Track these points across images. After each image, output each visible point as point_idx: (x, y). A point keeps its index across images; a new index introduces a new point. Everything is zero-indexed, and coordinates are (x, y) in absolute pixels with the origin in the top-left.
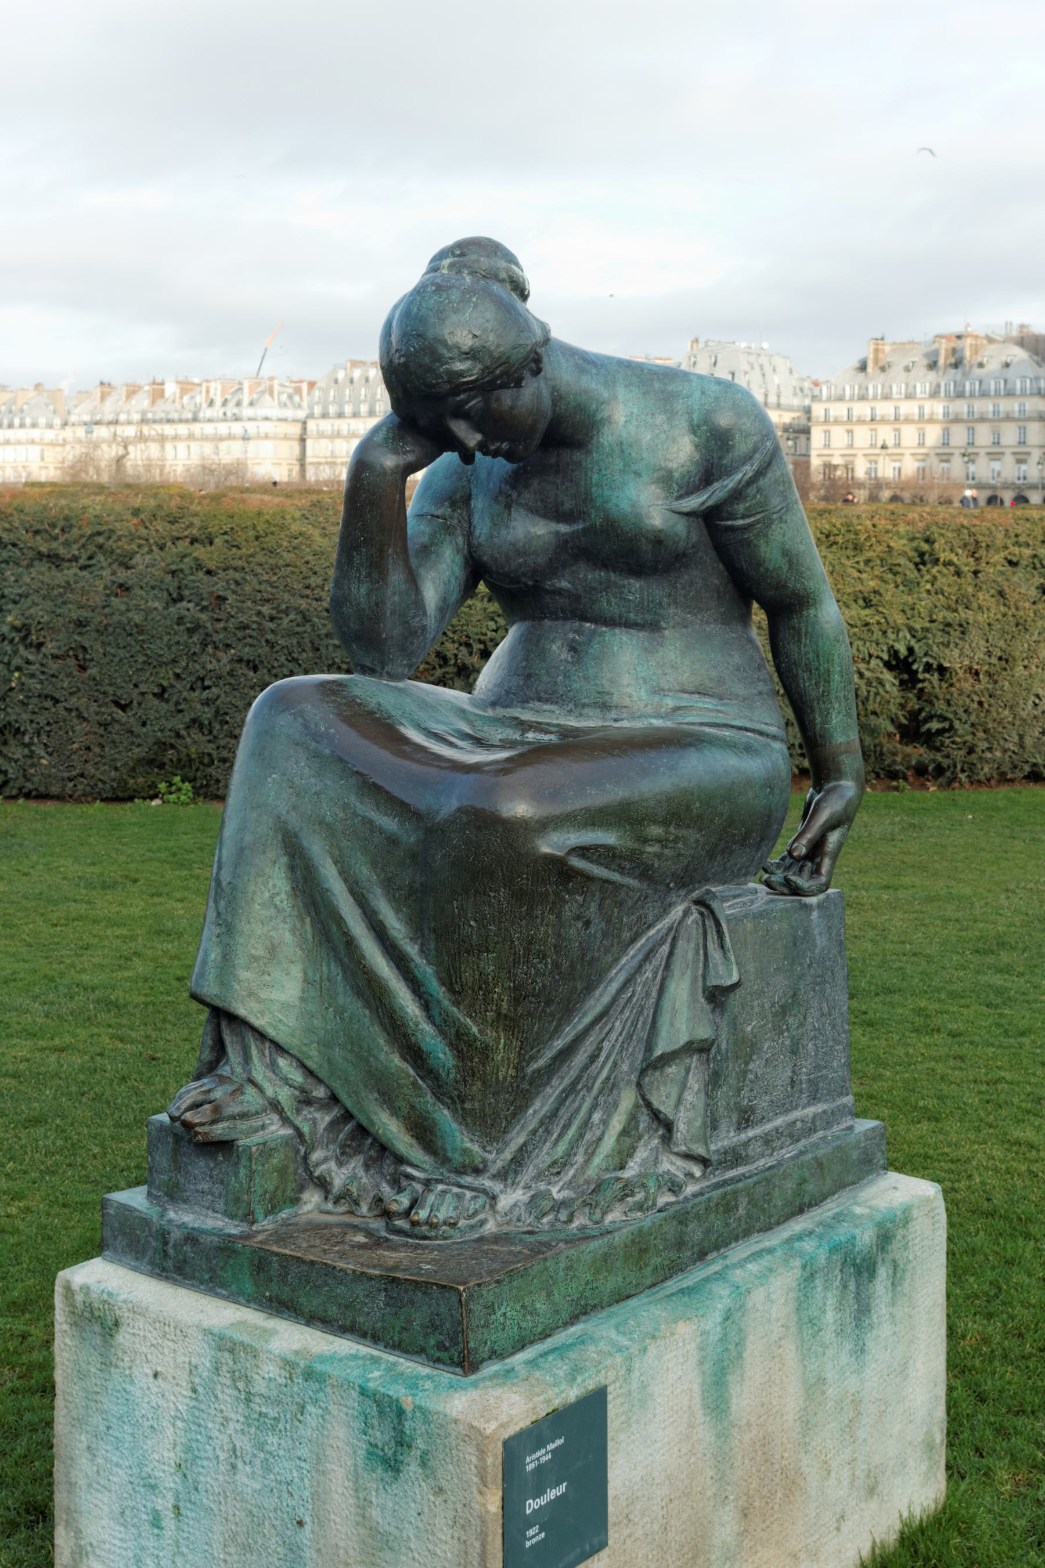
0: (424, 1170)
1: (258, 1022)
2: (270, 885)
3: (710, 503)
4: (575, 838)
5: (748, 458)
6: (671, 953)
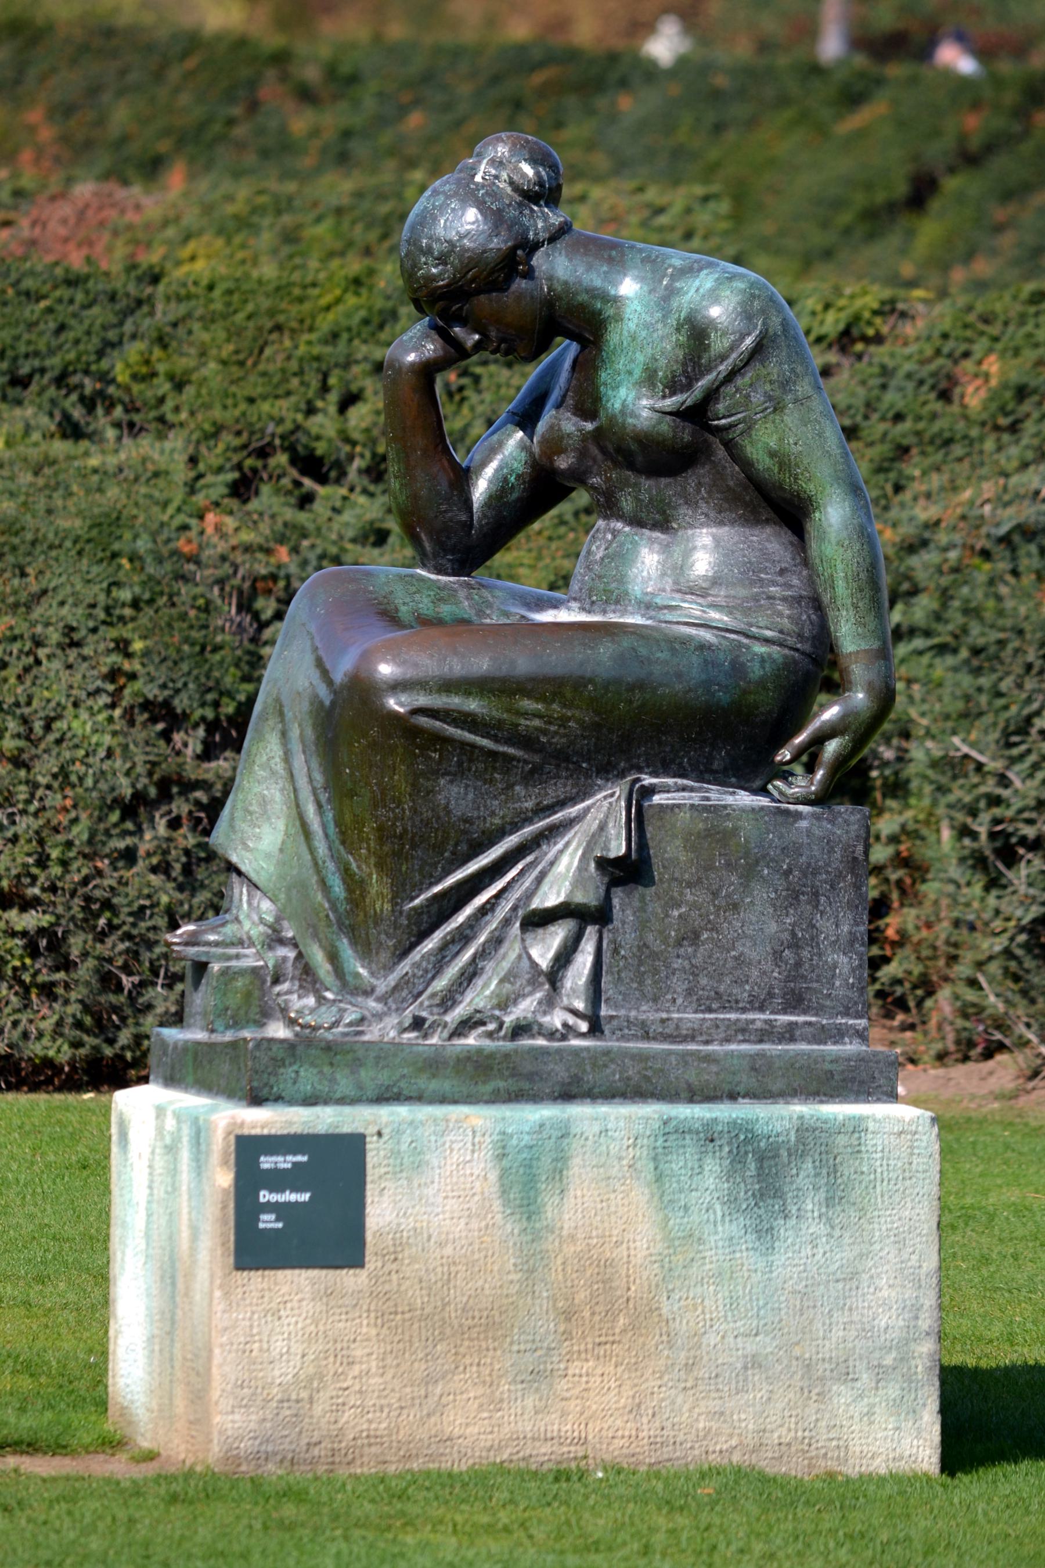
1: (243, 868)
3: (689, 403)
5: (723, 358)
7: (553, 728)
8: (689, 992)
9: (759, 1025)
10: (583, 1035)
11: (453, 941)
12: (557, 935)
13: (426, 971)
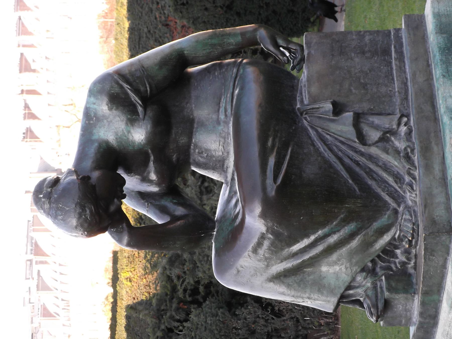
0: (397, 231)
2: (291, 283)
4: (270, 181)
5: (122, 87)
6: (320, 128)
7: (279, 135)
8: (386, 86)
9: (398, 63)
10: (409, 120)
11: (372, 176)
12: (366, 129)
13: (385, 186)
